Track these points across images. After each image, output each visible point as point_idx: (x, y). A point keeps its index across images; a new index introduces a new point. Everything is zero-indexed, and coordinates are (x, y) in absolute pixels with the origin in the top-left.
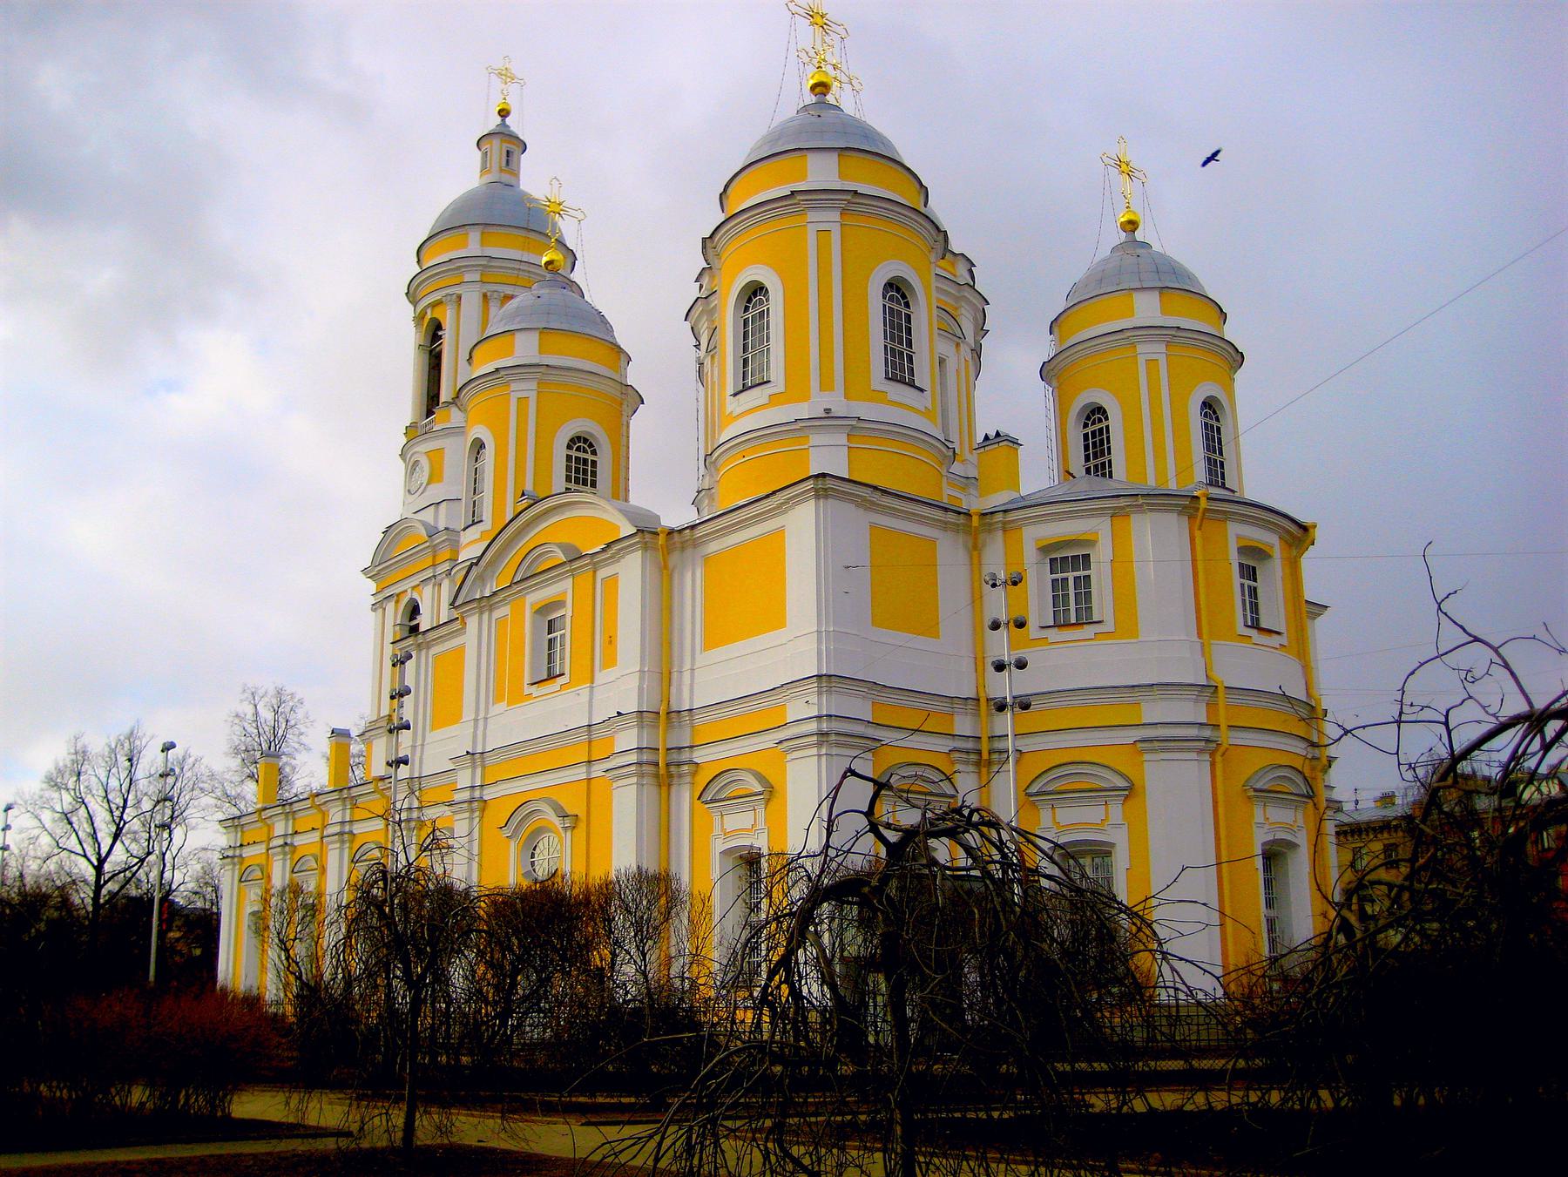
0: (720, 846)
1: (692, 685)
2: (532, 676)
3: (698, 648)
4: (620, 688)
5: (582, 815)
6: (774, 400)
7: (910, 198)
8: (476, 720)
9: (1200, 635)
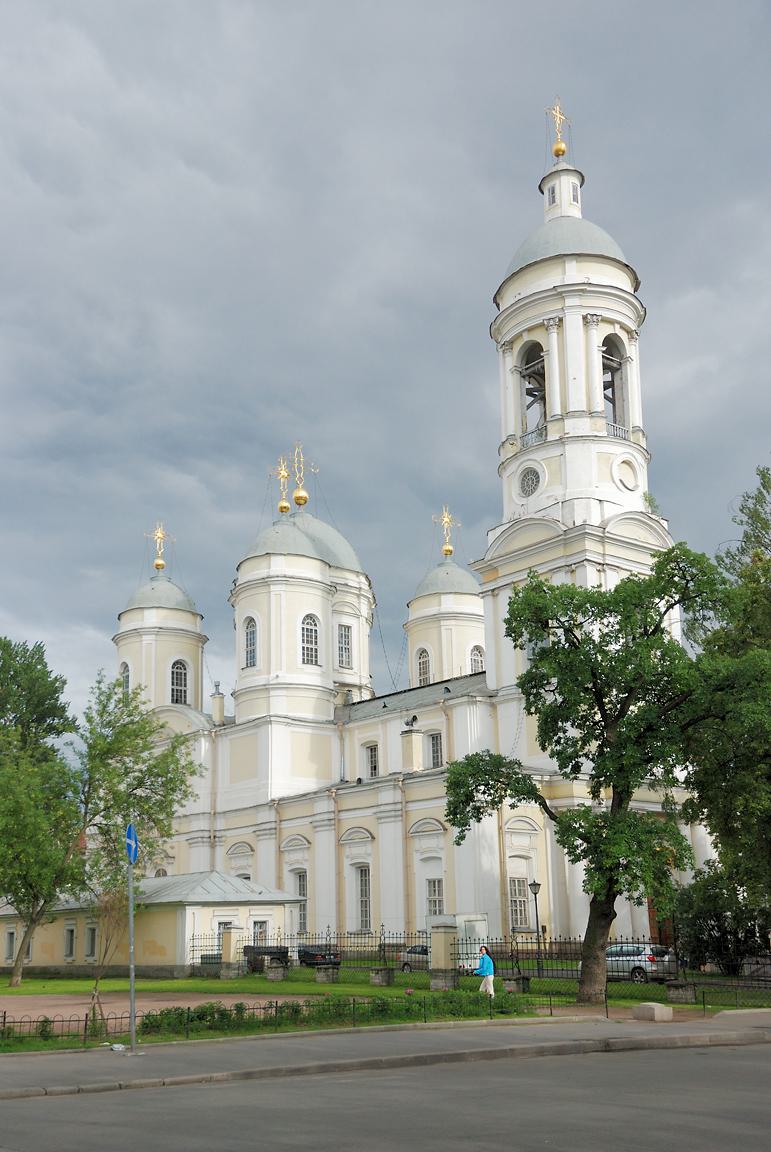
3: (609, 362)
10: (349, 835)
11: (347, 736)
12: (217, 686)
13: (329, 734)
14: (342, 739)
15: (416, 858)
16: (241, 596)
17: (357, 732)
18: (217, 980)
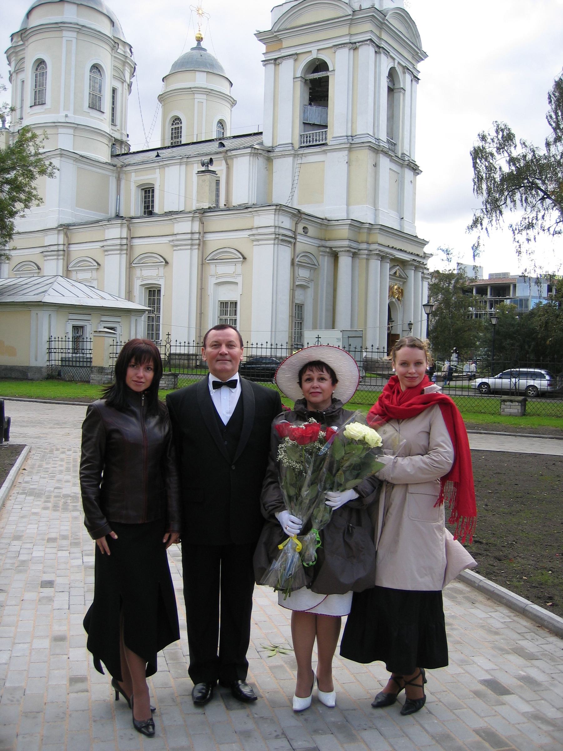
7: (277, 523)
10: (141, 259)
11: (123, 176)
12: (199, 40)
13: (110, 174)
14: (119, 180)
15: (211, 281)
16: (31, 40)
17: (133, 174)
18: (87, 386)
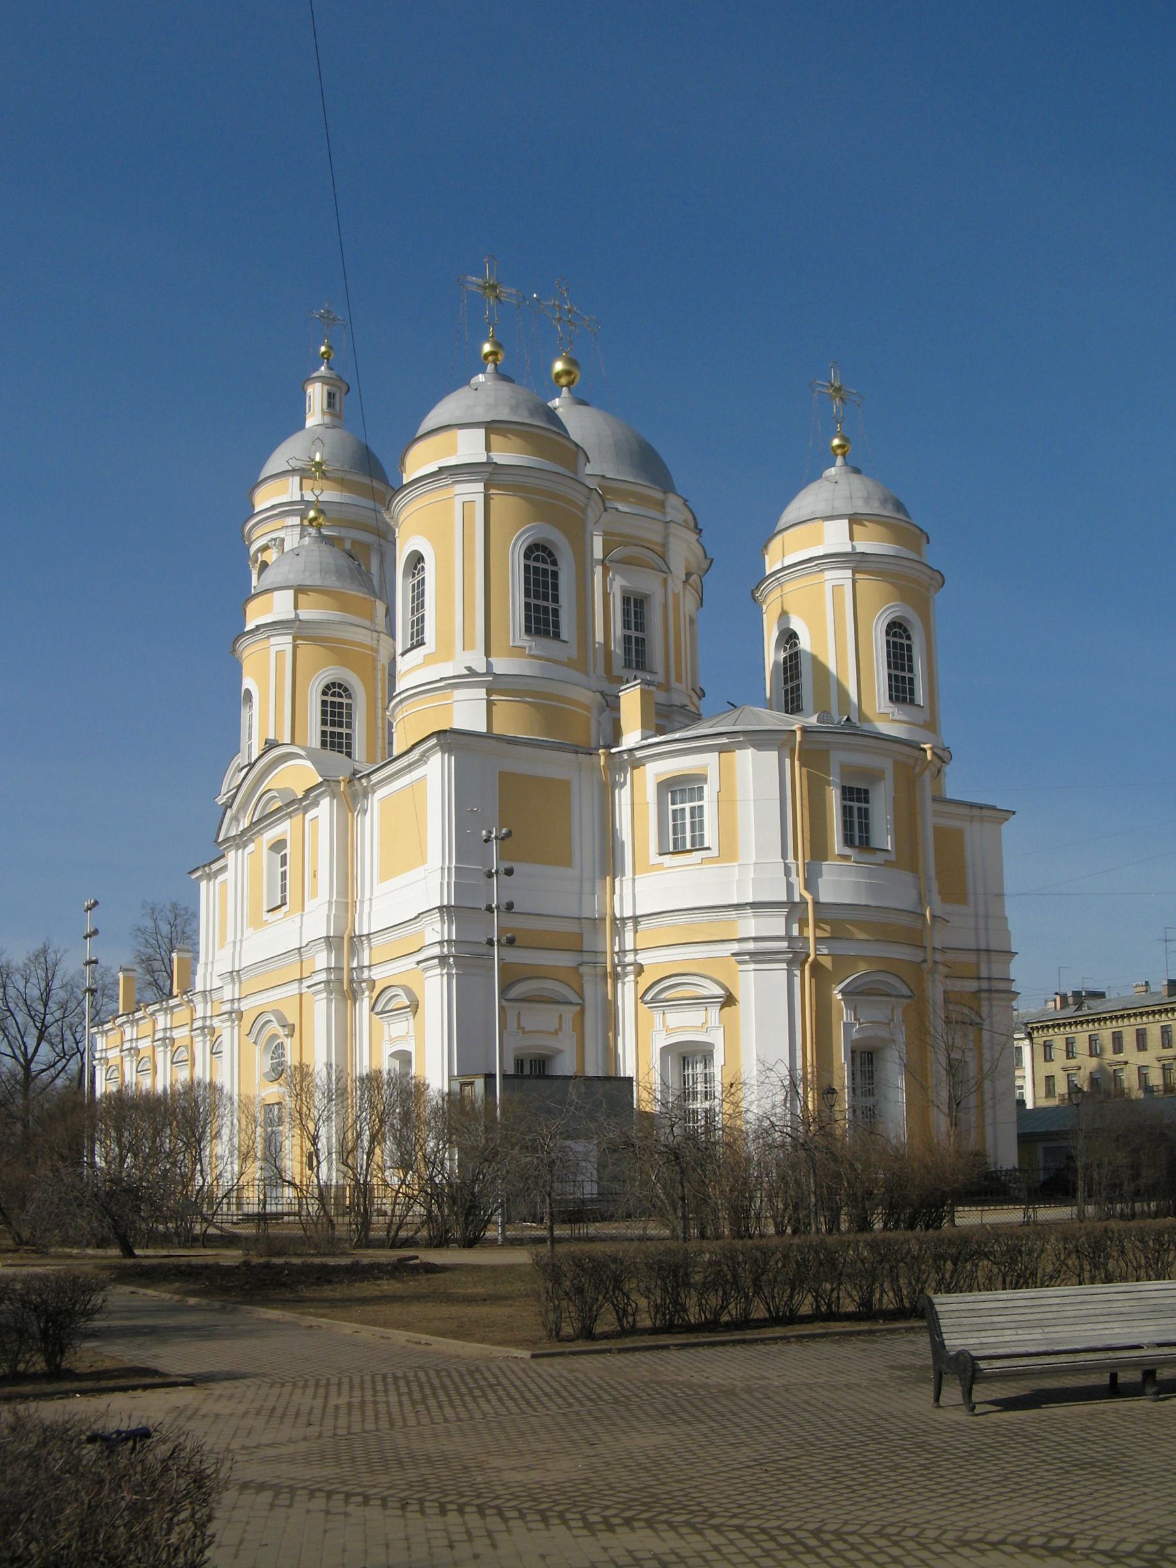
0: (662, 1040)
1: (370, 913)
2: (268, 905)
4: (315, 919)
5: (640, 1005)
6: (429, 660)
8: (235, 942)
9: (784, 856)
